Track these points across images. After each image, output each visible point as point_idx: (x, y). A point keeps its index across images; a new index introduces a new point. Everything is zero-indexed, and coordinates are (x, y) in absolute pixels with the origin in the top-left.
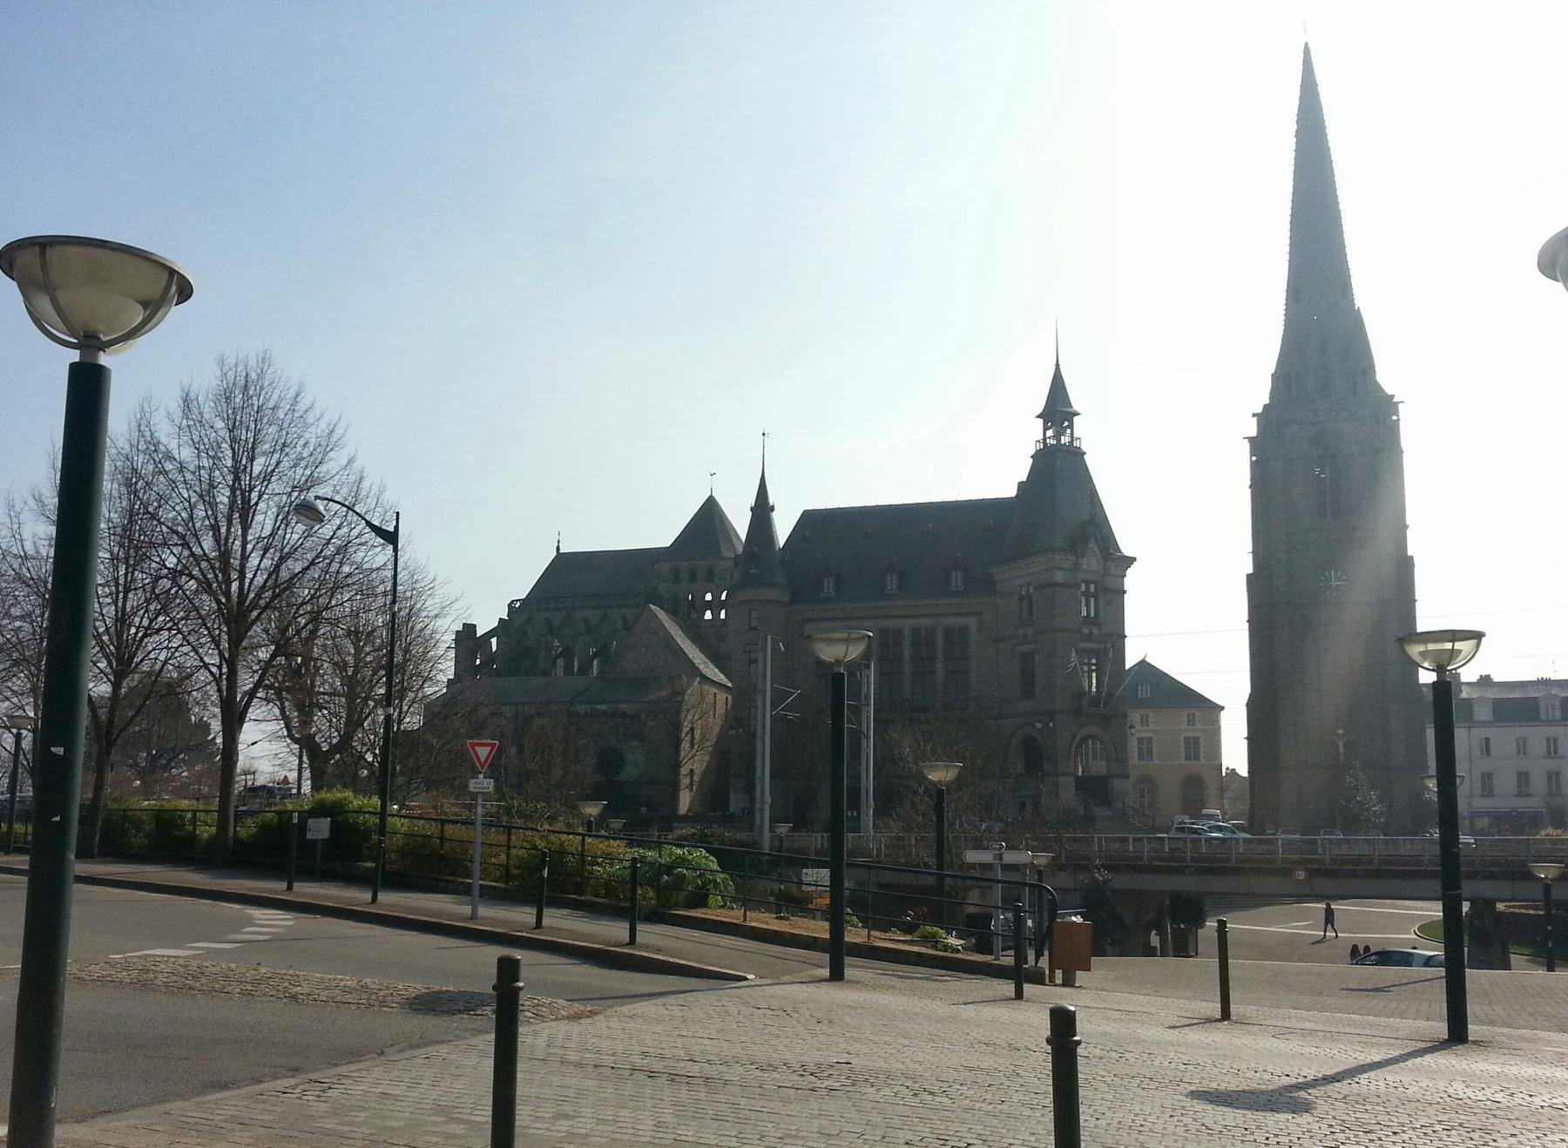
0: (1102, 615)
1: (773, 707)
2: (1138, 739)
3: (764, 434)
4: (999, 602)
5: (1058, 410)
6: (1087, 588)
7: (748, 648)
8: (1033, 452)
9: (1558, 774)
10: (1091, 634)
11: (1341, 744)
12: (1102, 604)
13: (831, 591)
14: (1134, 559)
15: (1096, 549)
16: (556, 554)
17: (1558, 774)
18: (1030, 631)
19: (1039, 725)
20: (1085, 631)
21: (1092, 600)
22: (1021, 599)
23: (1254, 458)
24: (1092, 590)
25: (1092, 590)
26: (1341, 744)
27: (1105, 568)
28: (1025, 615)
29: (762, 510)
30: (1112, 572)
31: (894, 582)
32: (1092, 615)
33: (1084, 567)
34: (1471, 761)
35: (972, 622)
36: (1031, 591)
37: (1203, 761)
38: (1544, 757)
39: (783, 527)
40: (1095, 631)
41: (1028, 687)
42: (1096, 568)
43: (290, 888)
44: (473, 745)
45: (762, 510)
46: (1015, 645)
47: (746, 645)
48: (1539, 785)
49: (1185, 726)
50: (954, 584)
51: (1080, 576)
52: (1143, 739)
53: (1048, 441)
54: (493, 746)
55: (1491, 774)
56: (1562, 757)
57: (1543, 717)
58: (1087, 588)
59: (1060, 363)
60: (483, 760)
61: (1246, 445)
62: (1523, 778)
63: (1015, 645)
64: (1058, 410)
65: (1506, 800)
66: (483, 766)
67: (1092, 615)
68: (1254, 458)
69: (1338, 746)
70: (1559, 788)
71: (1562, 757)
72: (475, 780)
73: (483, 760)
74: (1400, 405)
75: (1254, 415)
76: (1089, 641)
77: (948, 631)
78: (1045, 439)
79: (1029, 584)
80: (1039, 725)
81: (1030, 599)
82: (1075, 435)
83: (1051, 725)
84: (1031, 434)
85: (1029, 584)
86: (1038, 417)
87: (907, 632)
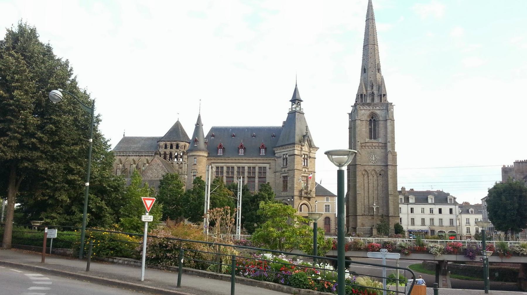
0: (309, 165)
1: (210, 191)
2: (325, 205)
3: (200, 100)
4: (276, 159)
5: (296, 100)
6: (305, 156)
7: (193, 171)
8: (288, 112)
9: (433, 219)
10: (305, 171)
11: (375, 208)
12: (309, 162)
13: (221, 153)
14: (318, 148)
15: (307, 144)
16: (123, 137)
17: (433, 219)
18: (286, 169)
19: (289, 200)
20: (304, 170)
21: (306, 160)
22: (284, 159)
23: (350, 120)
24: (306, 157)
25: (306, 157)
26: (375, 208)
27: (310, 150)
28: (285, 164)
29: (198, 126)
30: (312, 152)
31: (242, 151)
32: (306, 165)
33: (304, 150)
34: (408, 215)
35: (267, 166)
36: (287, 156)
37: (330, 212)
38: (429, 214)
39: (206, 131)
40: (307, 170)
41: (285, 187)
42: (307, 150)
43: (43, 260)
44: (144, 199)
45: (198, 126)
46: (281, 174)
47: (192, 170)
48: (427, 222)
49: (325, 201)
50: (262, 153)
51: (303, 152)
52: (327, 205)
53: (293, 109)
54: (153, 200)
55: (433, 219)
56: (434, 214)
57: (449, 202)
58: (305, 156)
59: (297, 84)
60: (149, 206)
61: (348, 116)
62: (423, 220)
63: (281, 174)
64: (296, 100)
65: (418, 227)
66: (148, 209)
67: (306, 165)
68: (350, 120)
69: (374, 209)
70: (433, 224)
71: (434, 214)
72: (145, 216)
73: (149, 206)
74: (394, 106)
75: (352, 106)
76: (305, 173)
77: (260, 168)
78: (292, 108)
79: (287, 154)
80: (289, 200)
81: (287, 159)
82: (301, 108)
83: (292, 200)
84: (288, 106)
85: (287, 154)
86: (290, 101)
87: (246, 168)
